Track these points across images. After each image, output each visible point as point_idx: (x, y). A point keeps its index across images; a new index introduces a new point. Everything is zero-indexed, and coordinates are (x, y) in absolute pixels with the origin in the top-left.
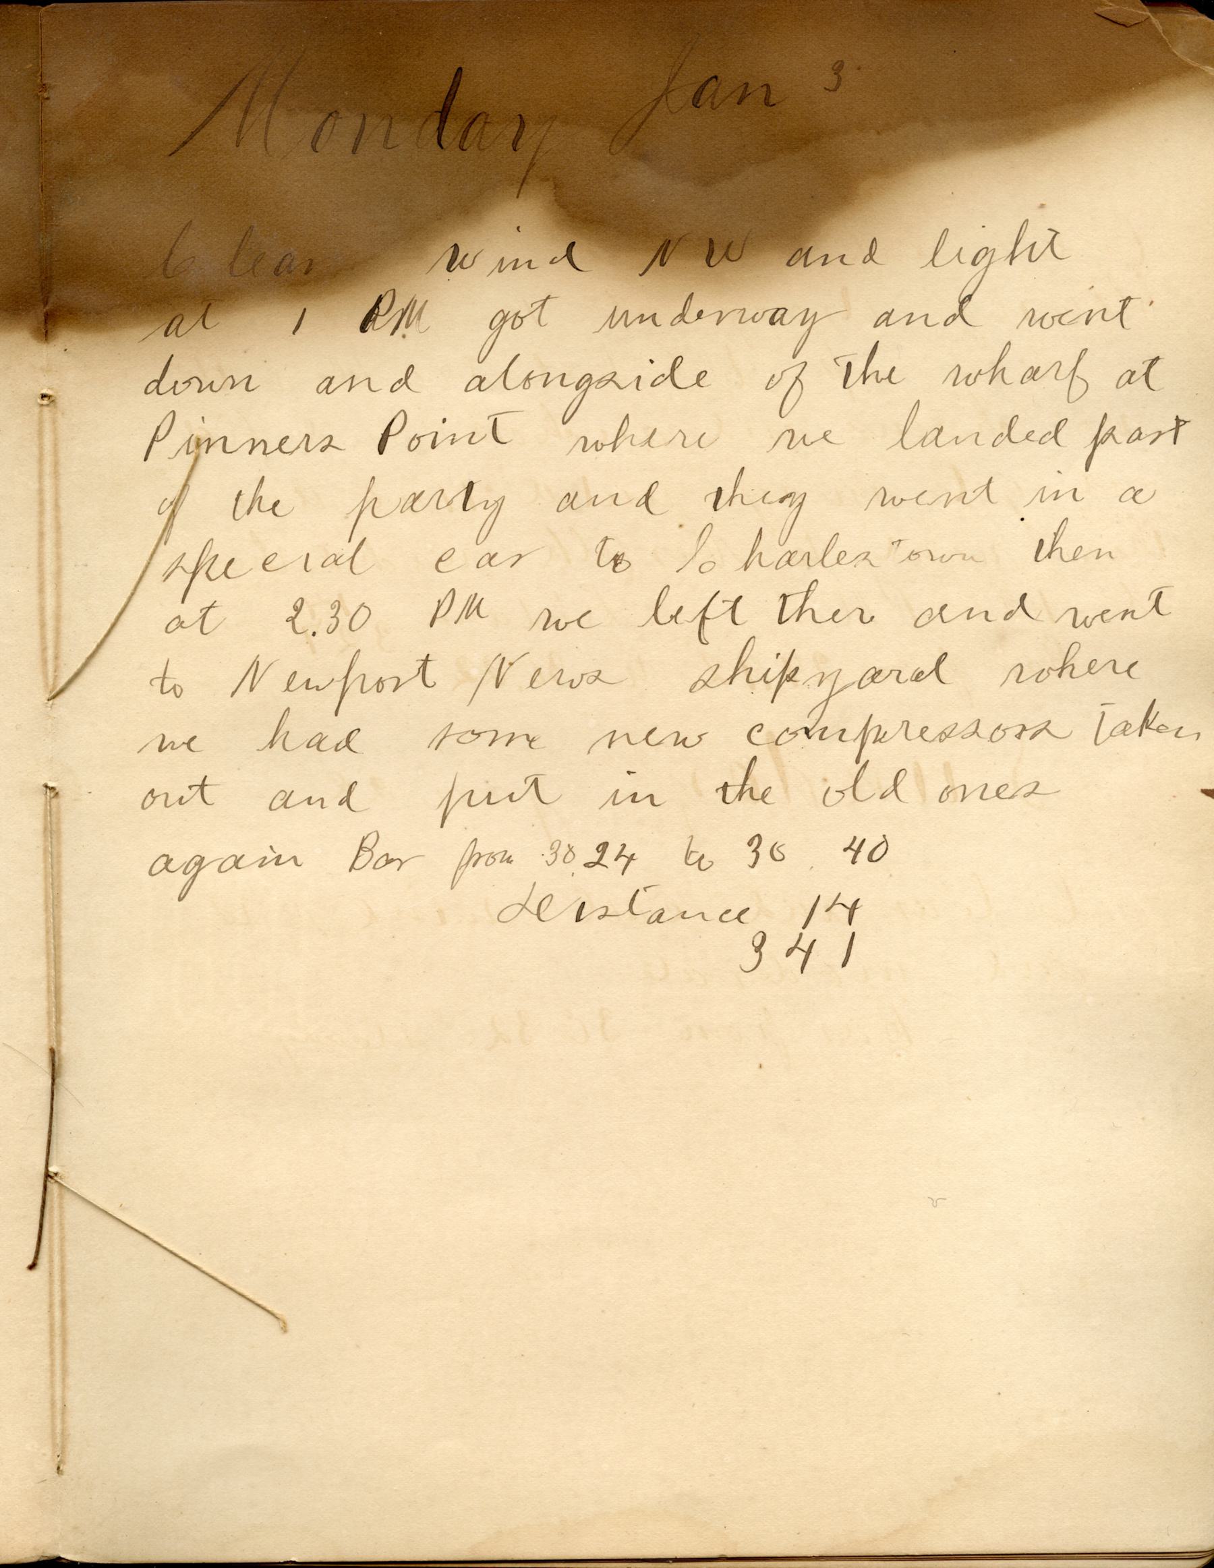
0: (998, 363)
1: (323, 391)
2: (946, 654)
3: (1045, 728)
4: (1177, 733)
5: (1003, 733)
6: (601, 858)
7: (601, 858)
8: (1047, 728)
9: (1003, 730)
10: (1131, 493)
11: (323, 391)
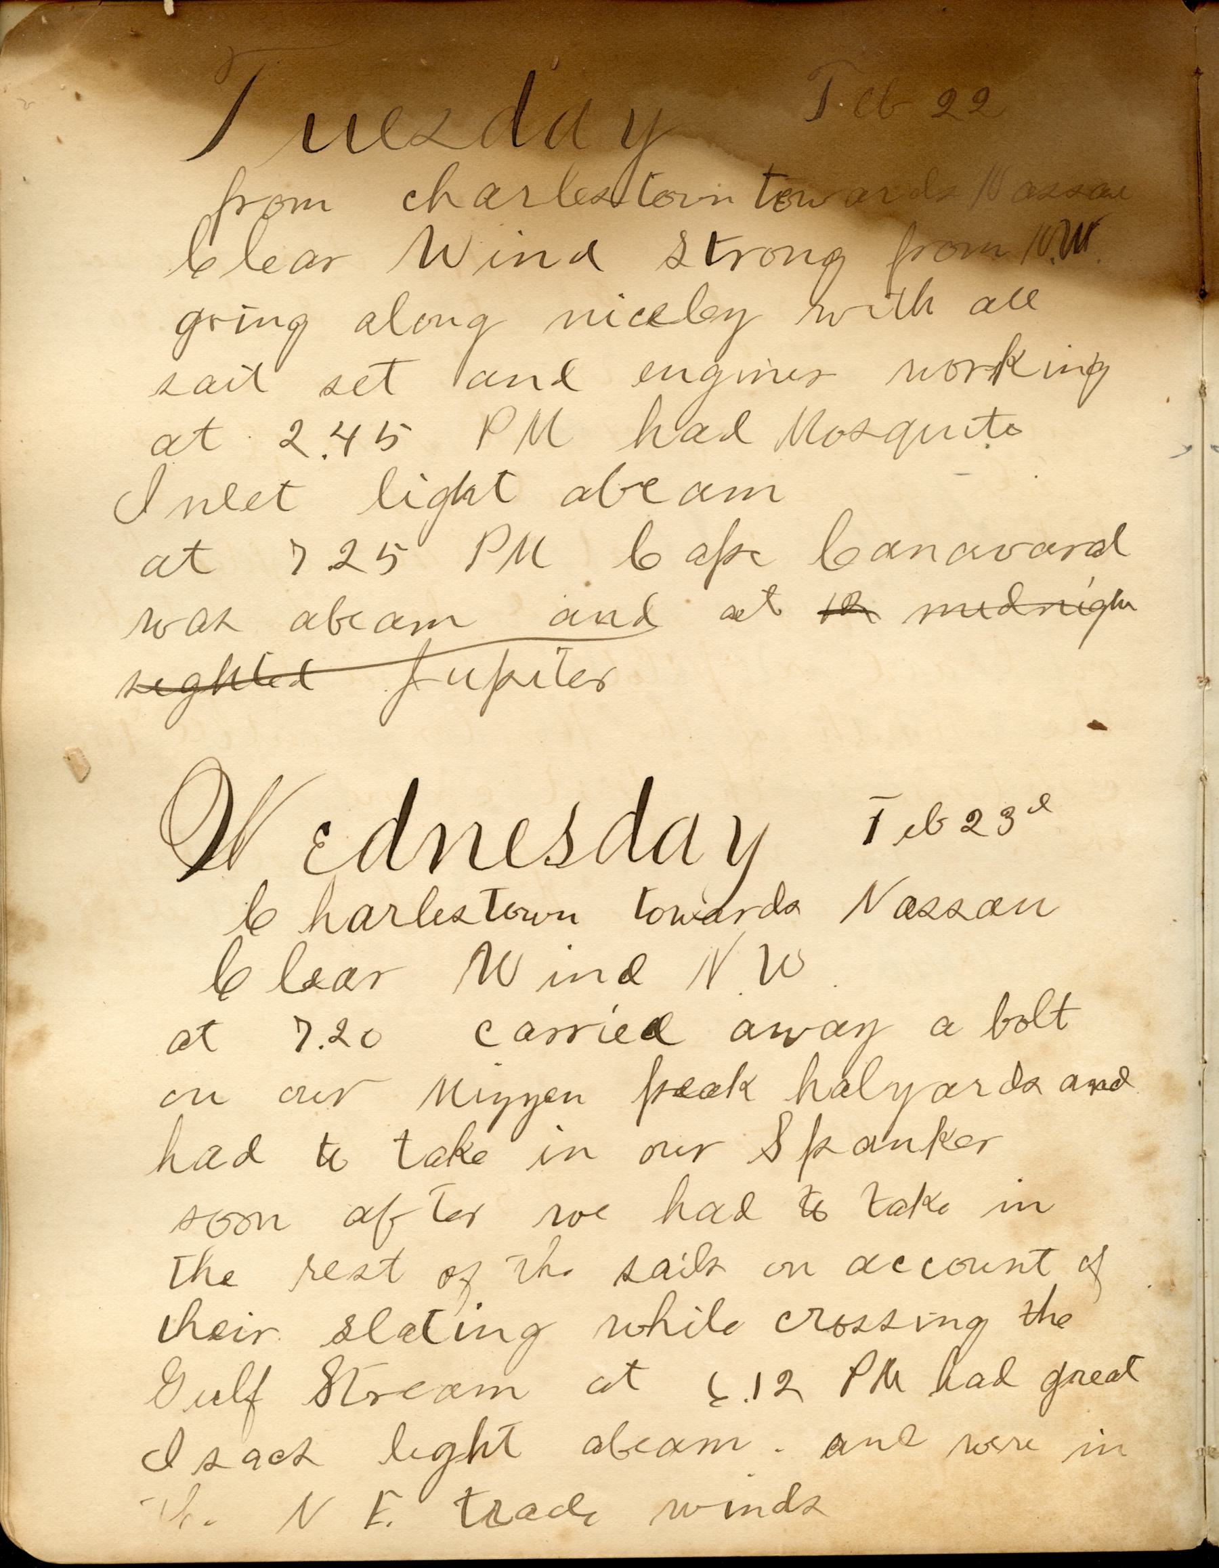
0: (642, 152)
1: (643, 917)
2: (656, 480)
3: (222, 622)
4: (478, 1099)
5: (939, 825)
6: (341, 1034)
7: (341, 1034)
8: (225, 620)
9: (940, 821)
10: (886, 548)
11: (643, 917)
